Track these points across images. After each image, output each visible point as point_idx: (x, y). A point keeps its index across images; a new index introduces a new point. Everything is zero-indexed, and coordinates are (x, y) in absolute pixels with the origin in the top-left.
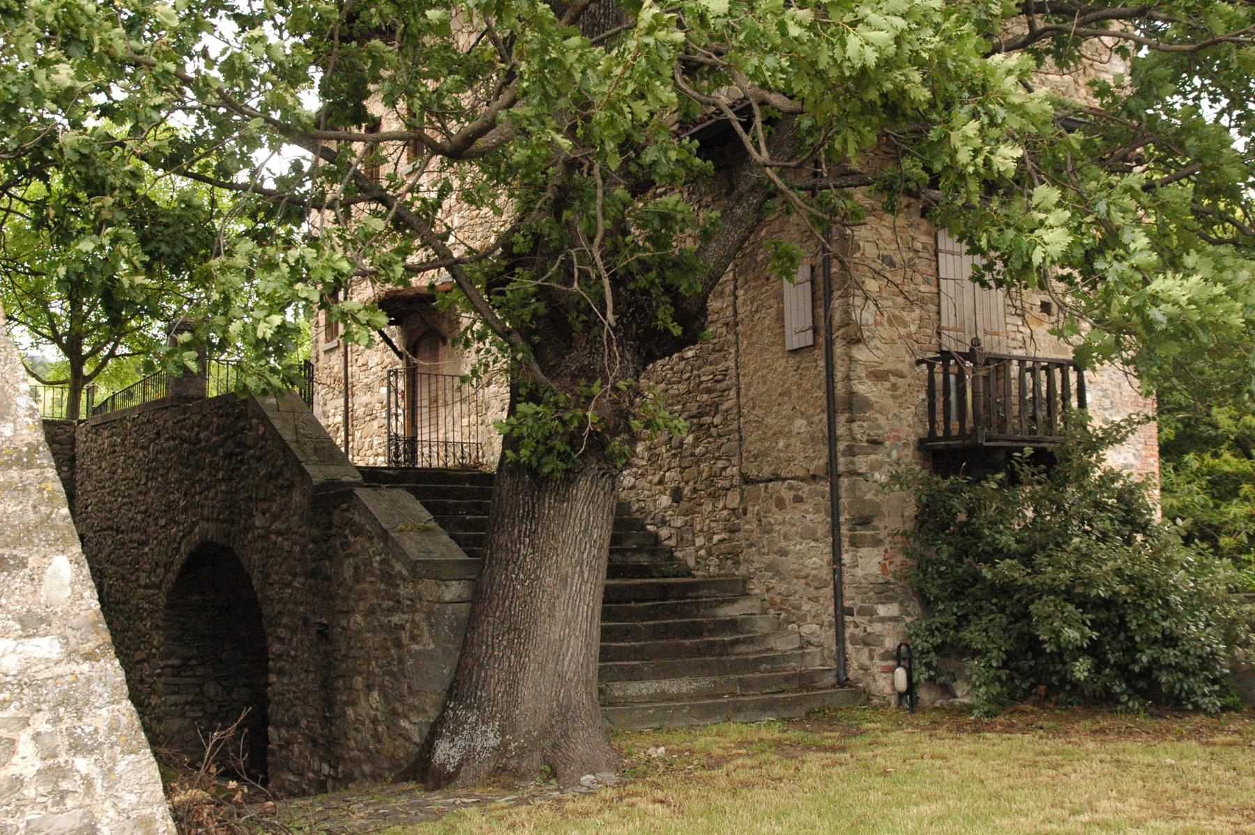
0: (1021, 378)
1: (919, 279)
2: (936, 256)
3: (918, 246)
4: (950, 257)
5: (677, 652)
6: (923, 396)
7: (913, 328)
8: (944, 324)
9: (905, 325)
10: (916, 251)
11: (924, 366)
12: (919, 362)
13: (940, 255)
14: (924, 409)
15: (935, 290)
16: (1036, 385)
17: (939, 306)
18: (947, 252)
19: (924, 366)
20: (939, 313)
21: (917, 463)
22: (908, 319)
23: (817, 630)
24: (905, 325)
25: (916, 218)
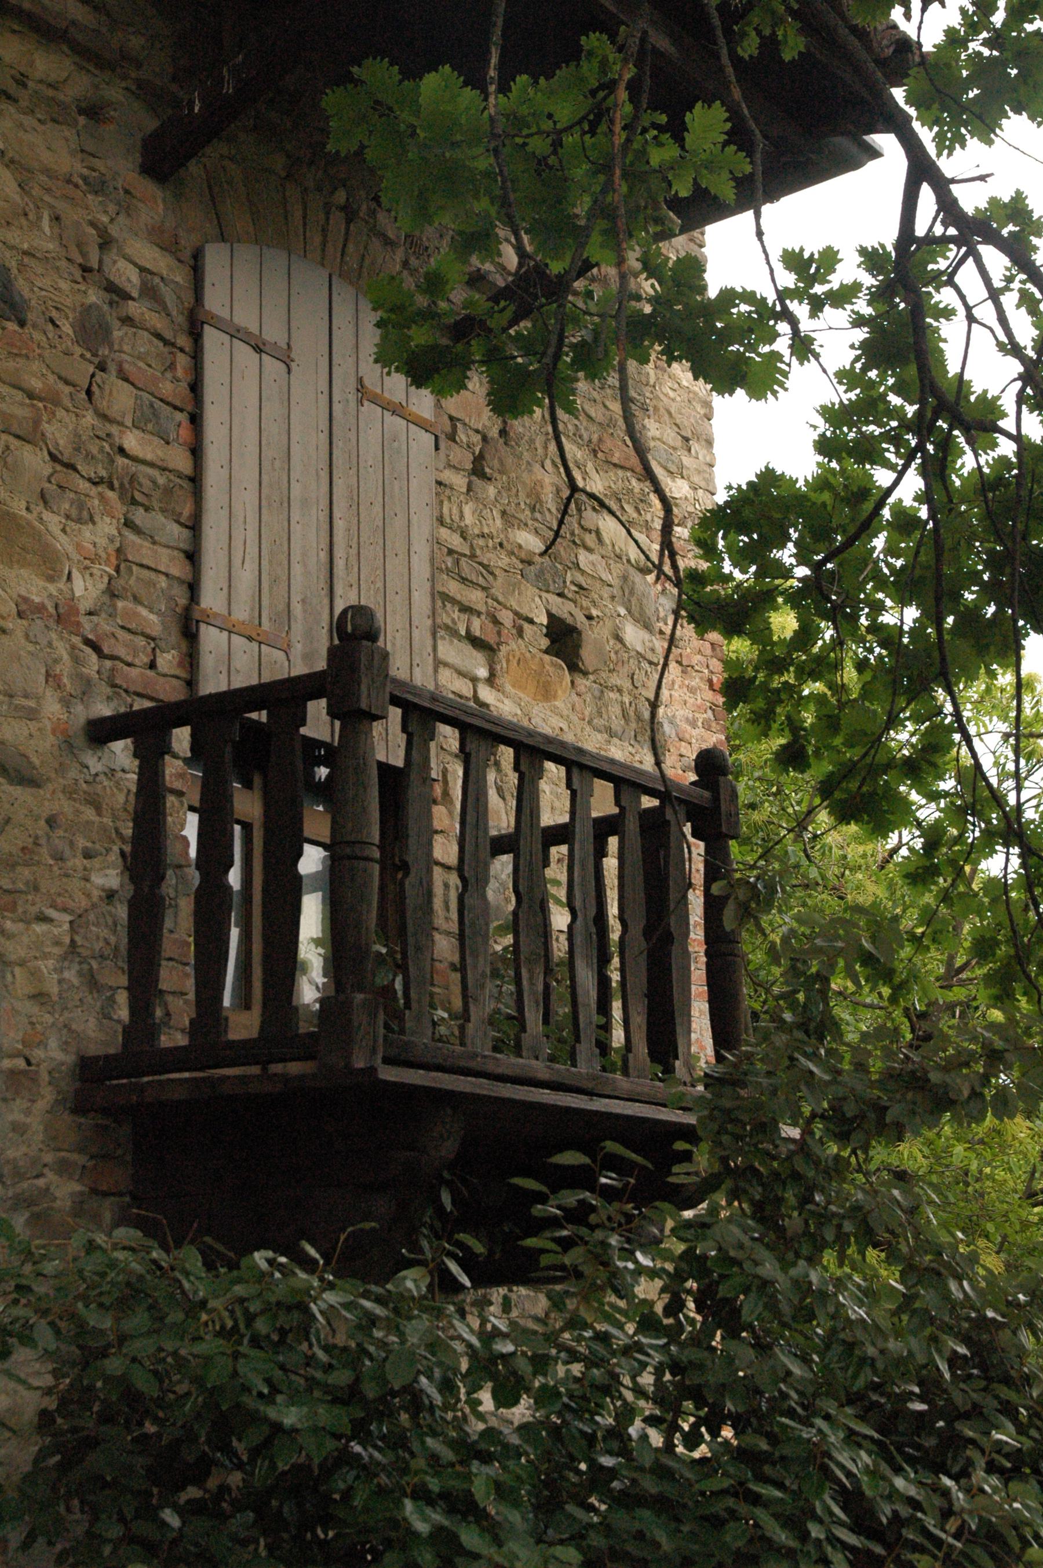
0: (470, 874)
1: (121, 399)
2: (197, 337)
3: (128, 276)
4: (244, 353)
5: (415, 695)
6: (110, 876)
7: (85, 589)
8: (211, 599)
9: (50, 565)
10: (116, 292)
11: (121, 750)
12: (100, 733)
13: (211, 337)
14: (110, 929)
15: (182, 462)
16: (531, 901)
17: (194, 526)
18: (236, 333)
19: (121, 750)
20: (193, 556)
21: (63, 1168)
22: (63, 543)
23: (834, 902)
24: (50, 565)
25: (124, 168)
